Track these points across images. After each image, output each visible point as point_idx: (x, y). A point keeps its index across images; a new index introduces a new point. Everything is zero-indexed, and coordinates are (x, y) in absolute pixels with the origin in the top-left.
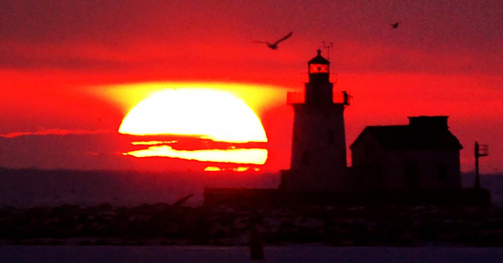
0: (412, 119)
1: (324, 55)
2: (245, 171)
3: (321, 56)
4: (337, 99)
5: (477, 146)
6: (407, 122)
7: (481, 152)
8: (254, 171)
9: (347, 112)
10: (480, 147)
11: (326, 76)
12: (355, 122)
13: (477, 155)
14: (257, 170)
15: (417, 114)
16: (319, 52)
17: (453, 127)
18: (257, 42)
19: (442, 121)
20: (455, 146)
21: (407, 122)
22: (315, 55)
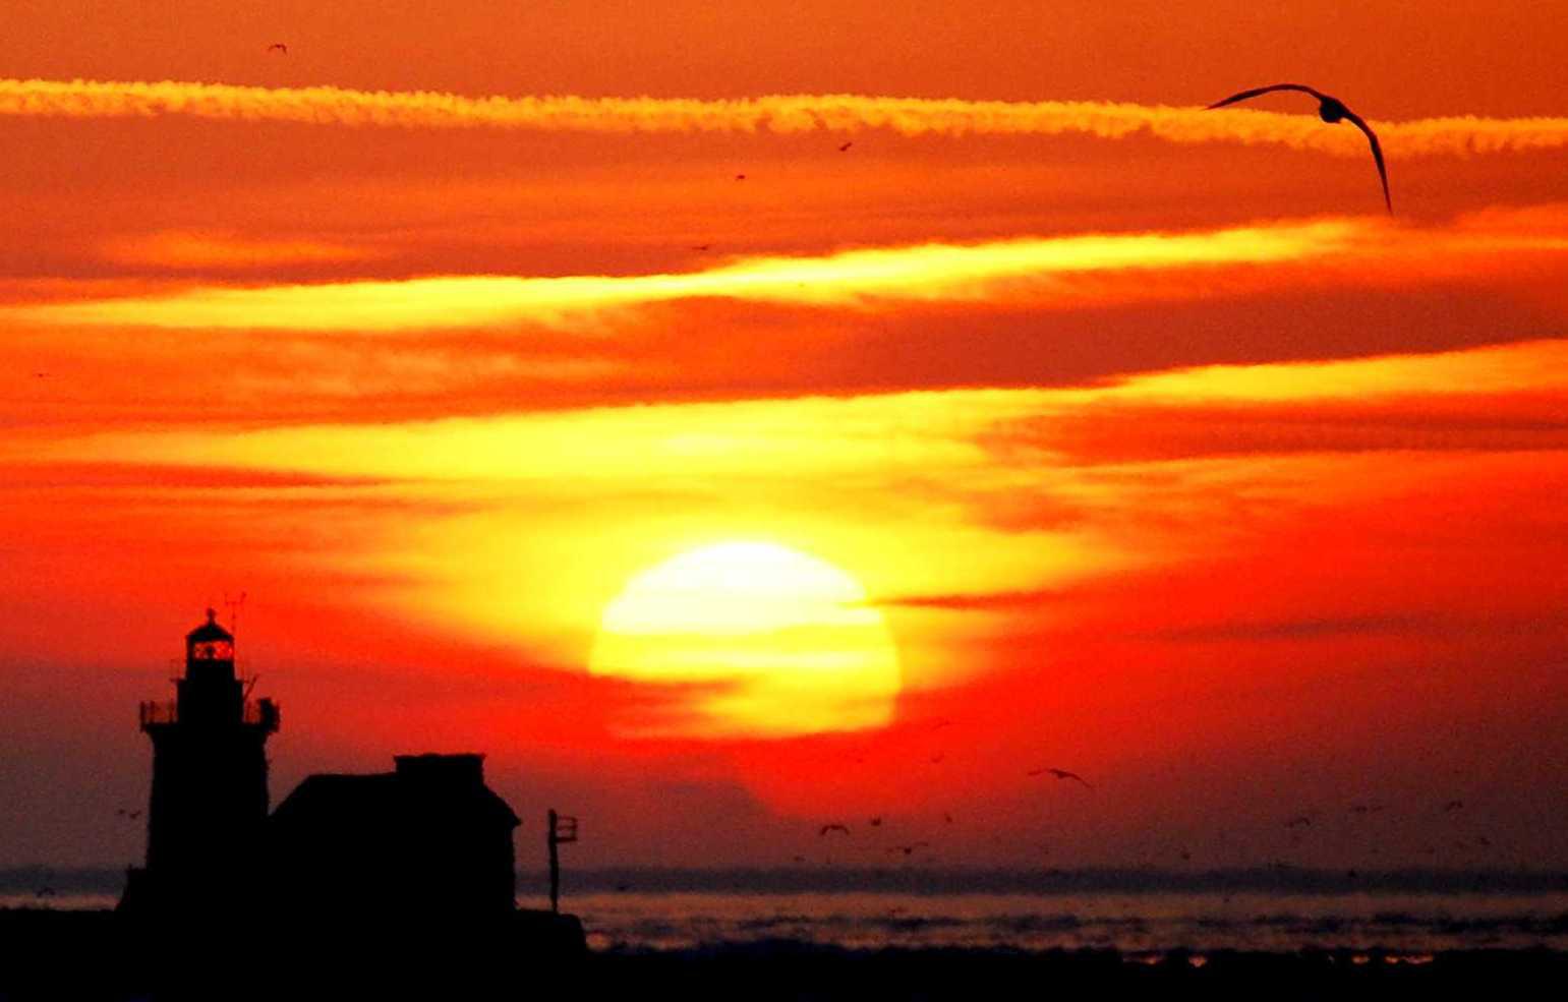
0: (403, 762)
1: (221, 621)
2: (1365, 964)
3: (214, 623)
4: (252, 715)
5: (553, 817)
6: (392, 768)
7: (559, 834)
8: (1193, 965)
9: (272, 745)
10: (560, 823)
11: (227, 666)
12: (286, 766)
13: (553, 841)
14: (1357, 960)
15: (417, 751)
16: (211, 613)
17: (494, 778)
18: (1038, 772)
19: (468, 766)
20: (500, 818)
21: (392, 768)
22: (202, 620)
